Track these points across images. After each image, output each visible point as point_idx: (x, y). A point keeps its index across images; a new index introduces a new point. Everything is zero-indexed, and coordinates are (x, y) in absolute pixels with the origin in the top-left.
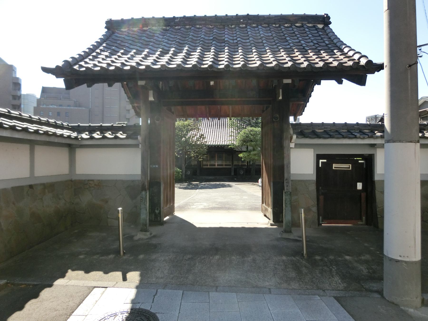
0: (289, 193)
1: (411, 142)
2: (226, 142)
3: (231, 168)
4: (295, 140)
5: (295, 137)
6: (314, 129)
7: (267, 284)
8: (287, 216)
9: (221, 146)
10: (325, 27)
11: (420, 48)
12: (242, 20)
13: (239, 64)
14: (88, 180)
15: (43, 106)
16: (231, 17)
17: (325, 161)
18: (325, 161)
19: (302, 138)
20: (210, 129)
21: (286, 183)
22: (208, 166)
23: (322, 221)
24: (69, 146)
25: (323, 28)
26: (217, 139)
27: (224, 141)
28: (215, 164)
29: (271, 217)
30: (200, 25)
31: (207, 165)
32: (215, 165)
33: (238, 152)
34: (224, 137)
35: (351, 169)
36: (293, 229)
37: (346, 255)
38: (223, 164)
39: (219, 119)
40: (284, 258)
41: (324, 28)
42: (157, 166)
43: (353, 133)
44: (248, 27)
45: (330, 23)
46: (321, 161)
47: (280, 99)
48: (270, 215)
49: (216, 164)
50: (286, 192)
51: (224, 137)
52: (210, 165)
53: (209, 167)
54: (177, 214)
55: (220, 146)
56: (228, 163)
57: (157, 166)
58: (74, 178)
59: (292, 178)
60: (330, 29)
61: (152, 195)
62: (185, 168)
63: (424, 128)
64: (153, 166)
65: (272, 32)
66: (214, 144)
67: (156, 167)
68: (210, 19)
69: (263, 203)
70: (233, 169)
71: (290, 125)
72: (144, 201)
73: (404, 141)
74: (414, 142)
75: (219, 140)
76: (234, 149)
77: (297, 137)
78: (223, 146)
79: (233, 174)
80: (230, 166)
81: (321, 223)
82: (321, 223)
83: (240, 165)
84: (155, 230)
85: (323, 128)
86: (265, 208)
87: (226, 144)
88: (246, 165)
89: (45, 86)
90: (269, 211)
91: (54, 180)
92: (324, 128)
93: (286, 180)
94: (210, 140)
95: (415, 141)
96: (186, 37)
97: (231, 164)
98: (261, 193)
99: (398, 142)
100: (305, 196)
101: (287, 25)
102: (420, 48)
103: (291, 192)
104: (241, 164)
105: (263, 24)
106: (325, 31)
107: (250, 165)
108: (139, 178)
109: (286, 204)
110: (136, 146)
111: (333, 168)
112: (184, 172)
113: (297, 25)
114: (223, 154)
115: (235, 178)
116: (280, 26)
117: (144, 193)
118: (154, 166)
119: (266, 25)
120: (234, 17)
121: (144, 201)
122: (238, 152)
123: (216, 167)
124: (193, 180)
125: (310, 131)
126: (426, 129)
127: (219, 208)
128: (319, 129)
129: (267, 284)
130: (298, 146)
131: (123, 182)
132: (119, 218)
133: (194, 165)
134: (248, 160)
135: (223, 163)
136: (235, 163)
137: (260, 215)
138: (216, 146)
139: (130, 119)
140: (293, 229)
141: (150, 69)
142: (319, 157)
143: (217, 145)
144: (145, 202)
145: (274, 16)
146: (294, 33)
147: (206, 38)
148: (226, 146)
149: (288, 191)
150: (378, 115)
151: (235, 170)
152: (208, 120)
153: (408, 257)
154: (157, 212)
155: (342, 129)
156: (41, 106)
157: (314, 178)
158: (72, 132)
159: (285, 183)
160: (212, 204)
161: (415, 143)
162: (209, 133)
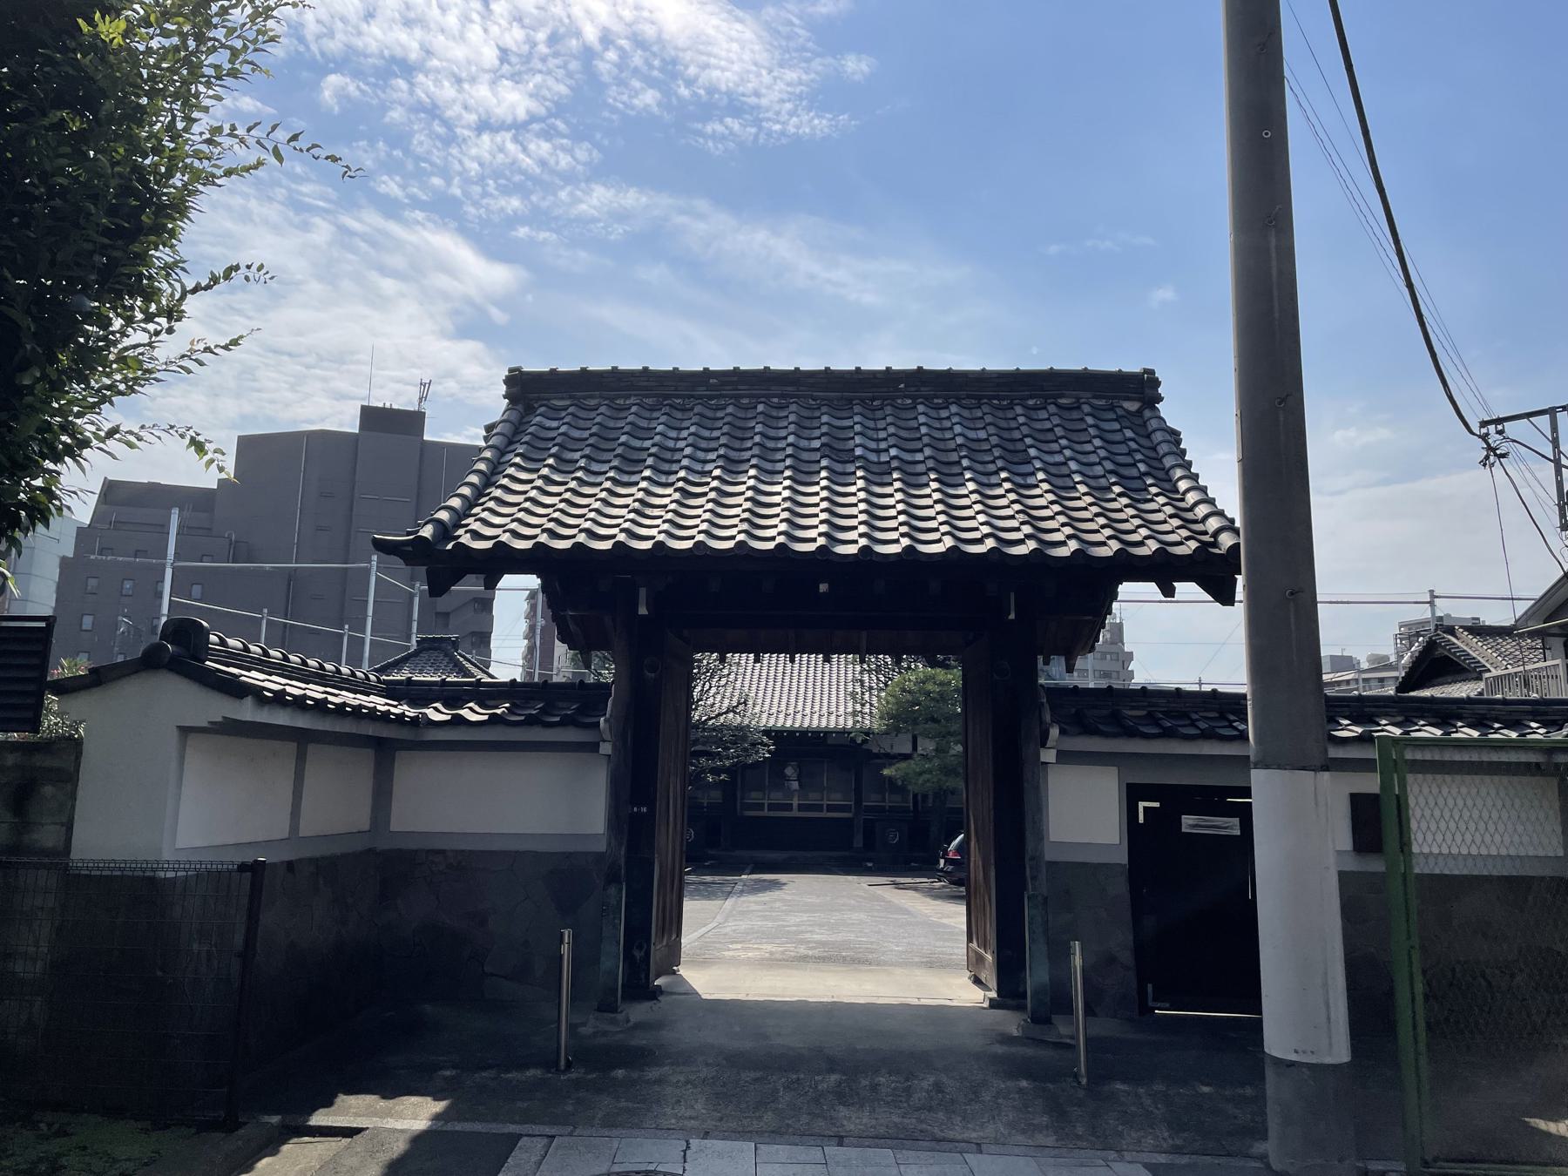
1: (1304, 769)
2: (833, 718)
4: (1057, 741)
5: (1054, 732)
7: (974, 1135)
8: (1036, 975)
9: (812, 732)
10: (1144, 410)
11: (1500, 427)
12: (902, 386)
13: (897, 541)
14: (428, 851)
15: (100, 557)
16: (872, 376)
17: (1157, 805)
18: (1157, 805)
19: (1080, 734)
21: (1031, 868)
22: (763, 810)
23: (1155, 1000)
24: (378, 744)
25: (1139, 412)
26: (800, 708)
28: (792, 804)
29: (993, 984)
30: (782, 396)
31: (760, 807)
33: (878, 756)
35: (1184, 833)
36: (1056, 1019)
37: (1202, 1085)
38: (823, 805)
39: (827, 660)
40: (1024, 1084)
41: (1141, 412)
42: (644, 810)
43: (1234, 724)
44: (921, 408)
45: (1160, 399)
46: (1142, 805)
48: (989, 975)
49: (795, 802)
50: (1033, 895)
52: (772, 807)
53: (766, 813)
54: (683, 971)
56: (837, 799)
57: (644, 810)
58: (383, 845)
59: (1050, 856)
60: (1157, 419)
63: (1461, 714)
65: (988, 428)
66: (788, 724)
68: (811, 381)
69: (970, 940)
71: (1043, 693)
72: (612, 916)
73: (1287, 767)
74: (1313, 770)
75: (808, 711)
76: (865, 747)
77: (1063, 732)
79: (858, 842)
81: (1150, 1004)
82: (1150, 1004)
83: (887, 808)
84: (639, 1012)
85: (1146, 704)
86: (977, 953)
87: (832, 725)
88: (912, 808)
90: (987, 962)
91: (336, 849)
92: (1149, 706)
93: (1032, 858)
94: (774, 710)
95: (1313, 768)
96: (743, 439)
97: (852, 803)
98: (964, 919)
99: (1275, 767)
101: (1034, 401)
102: (1500, 427)
103: (1047, 898)
104: (708, 803)
105: (964, 399)
106: (1144, 425)
108: (601, 847)
109: (1032, 932)
110: (593, 747)
111: (1184, 830)
113: (1063, 401)
115: (869, 861)
116: (1011, 403)
117: (612, 890)
118: (635, 809)
119: (973, 401)
120: (878, 376)
121: (612, 916)
122: (881, 758)
123: (795, 813)
125: (1105, 712)
126: (1464, 715)
127: (819, 958)
128: (1133, 708)
129: (974, 1135)
130: (1064, 757)
131: (537, 856)
132: (561, 957)
135: (822, 800)
136: (871, 800)
137: (964, 979)
138: (798, 734)
139: (451, 616)
140: (1056, 1019)
141: (664, 553)
142: (1134, 793)
144: (614, 918)
145: (996, 376)
146: (1051, 430)
147: (803, 443)
148: (834, 735)
150: (1448, 616)
152: (792, 661)
153: (1312, 1052)
154: (638, 958)
155: (1203, 710)
156: (92, 557)
157: (1122, 858)
158: (395, 703)
159: (1028, 870)
160: (795, 947)
161: (1313, 773)
162: (771, 684)
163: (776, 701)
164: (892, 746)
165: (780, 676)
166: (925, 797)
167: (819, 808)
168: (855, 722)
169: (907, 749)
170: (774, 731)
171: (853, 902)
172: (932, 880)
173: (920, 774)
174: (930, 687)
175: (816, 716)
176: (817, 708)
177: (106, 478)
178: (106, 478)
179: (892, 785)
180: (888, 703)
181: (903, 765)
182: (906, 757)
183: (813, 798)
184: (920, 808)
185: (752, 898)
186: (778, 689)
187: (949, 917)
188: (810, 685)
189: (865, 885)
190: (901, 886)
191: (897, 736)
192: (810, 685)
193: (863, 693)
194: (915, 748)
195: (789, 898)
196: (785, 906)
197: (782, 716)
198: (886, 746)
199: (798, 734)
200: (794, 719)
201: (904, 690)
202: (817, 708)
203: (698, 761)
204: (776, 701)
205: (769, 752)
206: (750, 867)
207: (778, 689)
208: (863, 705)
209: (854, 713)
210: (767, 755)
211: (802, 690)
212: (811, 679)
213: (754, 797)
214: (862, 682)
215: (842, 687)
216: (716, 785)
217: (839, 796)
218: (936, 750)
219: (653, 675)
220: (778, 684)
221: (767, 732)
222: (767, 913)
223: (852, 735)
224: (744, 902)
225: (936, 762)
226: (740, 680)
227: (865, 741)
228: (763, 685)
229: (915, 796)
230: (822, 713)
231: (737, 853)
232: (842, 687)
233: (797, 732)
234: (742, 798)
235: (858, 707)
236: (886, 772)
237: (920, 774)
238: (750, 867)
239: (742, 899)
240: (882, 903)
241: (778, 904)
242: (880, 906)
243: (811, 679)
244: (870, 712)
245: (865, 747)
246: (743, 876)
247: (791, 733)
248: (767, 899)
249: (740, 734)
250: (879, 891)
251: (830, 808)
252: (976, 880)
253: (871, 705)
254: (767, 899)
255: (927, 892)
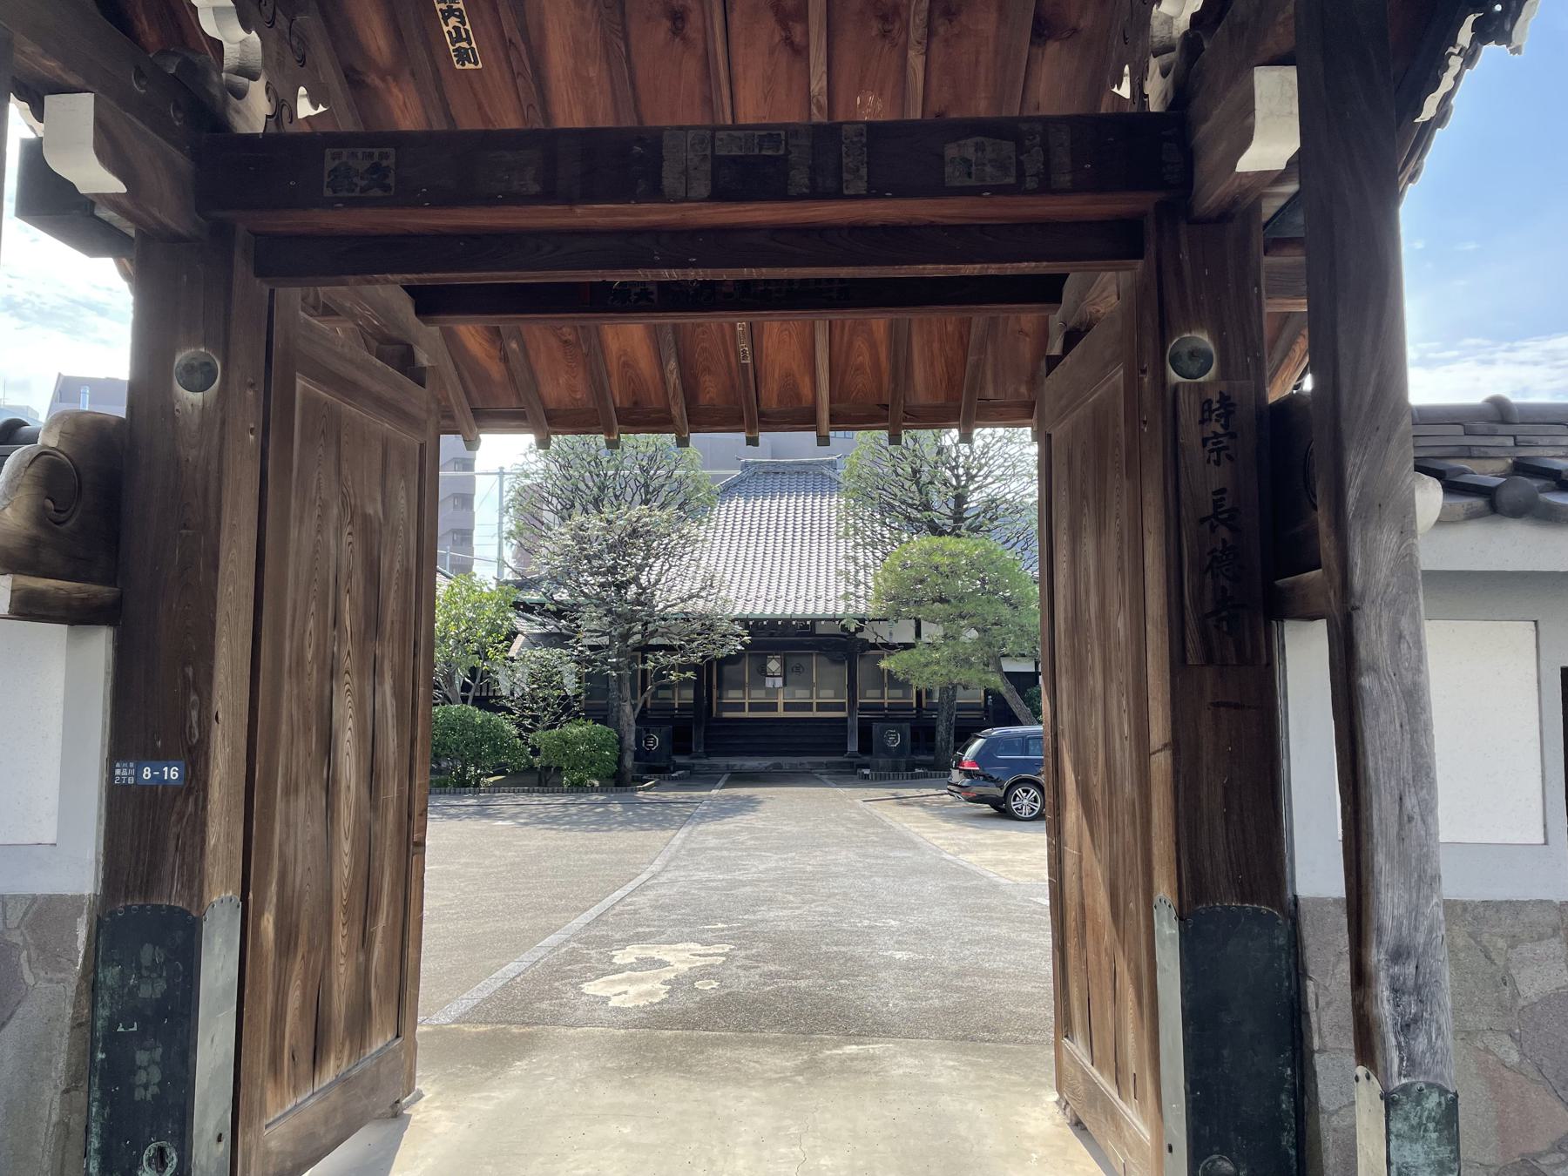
0: (1432, 1101)
2: (821, 603)
3: (844, 720)
6: (1524, 453)
9: (797, 620)
20: (752, 546)
26: (783, 592)
27: (813, 599)
31: (740, 707)
32: (774, 707)
33: (874, 646)
34: (813, 584)
42: (173, 773)
47: (1245, 175)
49: (781, 701)
50: (1405, 1089)
51: (813, 584)
52: (753, 707)
55: (794, 623)
56: (827, 695)
57: (173, 773)
61: (120, 1029)
62: (632, 722)
64: (138, 775)
67: (166, 784)
70: (853, 725)
75: (792, 595)
76: (859, 635)
78: (808, 623)
79: (853, 746)
80: (844, 710)
83: (886, 706)
88: (915, 705)
89: (66, 373)
94: (752, 595)
97: (846, 701)
100: (1487, 1050)
107: (934, 708)
112: (631, 739)
114: (812, 654)
118: (147, 773)
122: (878, 649)
124: (675, 779)
133: (683, 707)
134: (922, 685)
136: (870, 696)
138: (780, 623)
143: (783, 617)
148: (823, 622)
149: (1420, 1081)
151: (865, 731)
162: (749, 566)
163: (755, 584)
164: (891, 634)
165: (760, 555)
166: (929, 693)
167: (808, 707)
168: (848, 606)
169: (909, 638)
170: (751, 620)
171: (842, 829)
172: (939, 792)
173: (926, 665)
174: (937, 559)
175: (801, 602)
176: (802, 592)
177: (60, 374)
178: (60, 374)
179: (892, 680)
180: (885, 580)
181: (905, 654)
182: (907, 646)
183: (801, 695)
184: (924, 705)
185: (713, 827)
186: (757, 572)
187: (968, 851)
188: (795, 567)
189: (859, 801)
190: (904, 801)
191: (896, 621)
192: (795, 567)
193: (857, 572)
194: (918, 634)
195: (760, 825)
196: (752, 839)
197: (761, 602)
198: (884, 633)
199: (780, 623)
200: (775, 605)
201: (904, 566)
202: (802, 592)
203: (655, 655)
204: (755, 584)
205: (742, 644)
206: (725, 777)
207: (757, 572)
208: (857, 586)
209: (846, 596)
210: (739, 647)
211: (786, 573)
212: (796, 560)
213: (733, 695)
214: (855, 559)
215: (833, 564)
216: (684, 683)
217: (831, 693)
218: (945, 637)
219: (197, 397)
220: (758, 567)
221: (744, 621)
222: (725, 853)
223: (843, 622)
224: (700, 833)
225: (946, 652)
226: (705, 559)
227: (860, 629)
228: (739, 568)
229: (919, 694)
230: (808, 598)
231: (715, 760)
232: (833, 564)
233: (780, 620)
234: (720, 697)
235: (851, 589)
236: (883, 664)
237: (926, 665)
238: (725, 777)
239: (702, 827)
240: (880, 830)
241: (743, 837)
242: (876, 834)
243: (796, 560)
244: (865, 595)
245: (859, 635)
246: (714, 792)
247: (773, 622)
248: (731, 826)
249: (708, 625)
250: (877, 810)
251: (821, 707)
252: (1082, 907)
253: (867, 587)
254: (731, 826)
255: (938, 808)
